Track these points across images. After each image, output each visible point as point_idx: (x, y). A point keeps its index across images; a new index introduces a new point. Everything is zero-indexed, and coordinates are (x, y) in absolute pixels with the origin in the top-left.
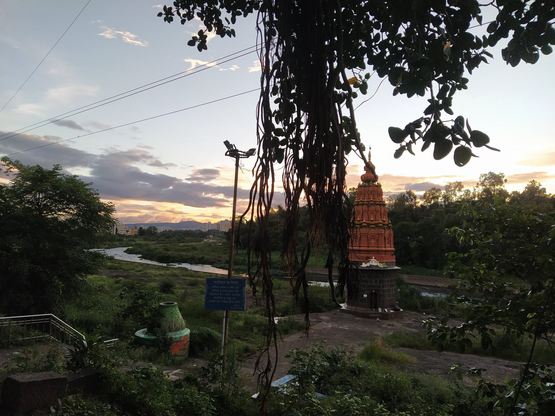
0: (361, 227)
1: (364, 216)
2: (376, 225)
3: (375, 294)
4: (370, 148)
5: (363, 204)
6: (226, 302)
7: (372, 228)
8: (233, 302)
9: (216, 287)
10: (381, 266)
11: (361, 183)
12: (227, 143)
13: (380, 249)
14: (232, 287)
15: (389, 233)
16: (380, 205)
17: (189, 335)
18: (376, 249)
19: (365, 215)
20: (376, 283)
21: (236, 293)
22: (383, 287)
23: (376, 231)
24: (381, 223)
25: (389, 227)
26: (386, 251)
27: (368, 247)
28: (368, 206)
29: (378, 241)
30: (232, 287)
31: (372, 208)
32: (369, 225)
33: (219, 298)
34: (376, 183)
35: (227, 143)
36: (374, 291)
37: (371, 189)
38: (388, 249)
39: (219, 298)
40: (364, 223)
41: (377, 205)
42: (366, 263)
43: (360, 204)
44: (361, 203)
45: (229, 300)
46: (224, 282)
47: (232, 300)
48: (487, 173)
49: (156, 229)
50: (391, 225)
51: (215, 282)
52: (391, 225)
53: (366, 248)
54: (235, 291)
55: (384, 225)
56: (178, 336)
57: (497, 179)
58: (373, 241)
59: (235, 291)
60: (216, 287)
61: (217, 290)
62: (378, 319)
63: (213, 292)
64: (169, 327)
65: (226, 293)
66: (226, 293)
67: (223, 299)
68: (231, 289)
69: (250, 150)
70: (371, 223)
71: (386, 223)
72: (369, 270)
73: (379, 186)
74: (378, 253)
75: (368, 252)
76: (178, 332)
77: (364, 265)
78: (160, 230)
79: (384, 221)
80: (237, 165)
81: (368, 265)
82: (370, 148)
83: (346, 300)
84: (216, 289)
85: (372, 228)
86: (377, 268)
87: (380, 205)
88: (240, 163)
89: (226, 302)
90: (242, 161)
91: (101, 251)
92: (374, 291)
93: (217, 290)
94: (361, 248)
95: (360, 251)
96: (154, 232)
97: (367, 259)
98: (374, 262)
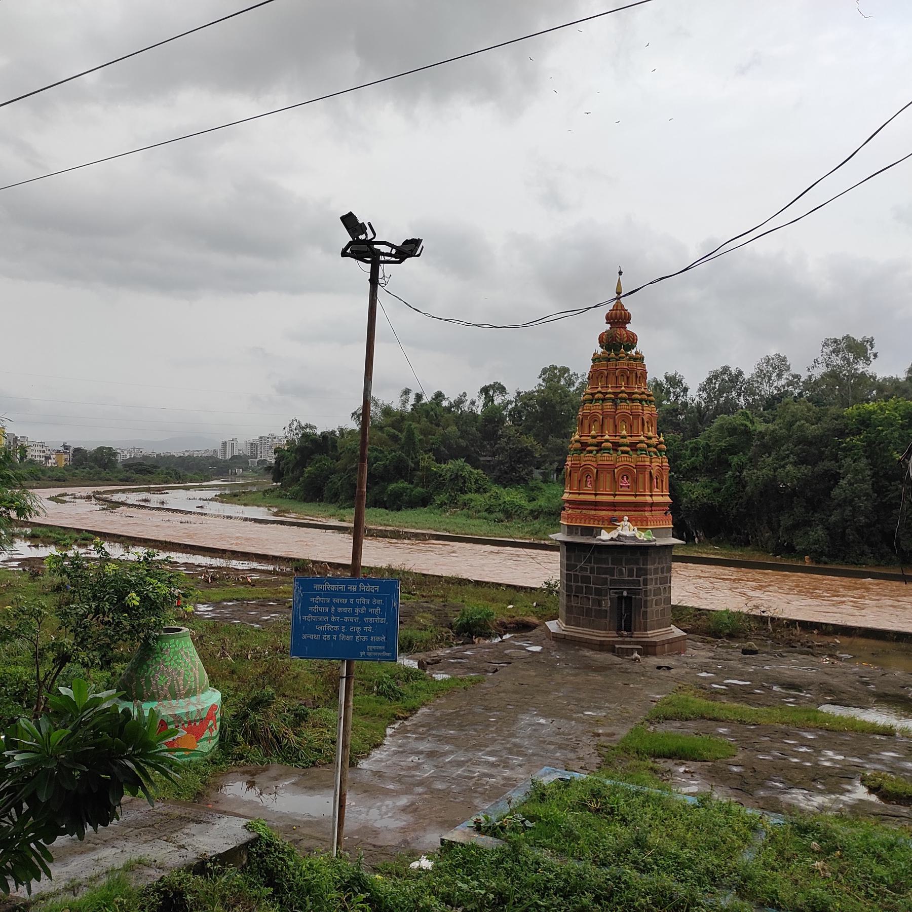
0: (598, 452)
1: (606, 427)
2: (633, 446)
3: (629, 599)
4: (620, 273)
5: (604, 400)
6: (349, 638)
7: (623, 452)
8: (365, 638)
9: (323, 600)
10: (643, 537)
11: (600, 351)
12: (349, 221)
13: (639, 499)
14: (363, 600)
15: (658, 463)
16: (641, 401)
17: (219, 705)
18: (632, 499)
19: (609, 423)
20: (631, 575)
21: (374, 616)
22: (645, 584)
23: (631, 460)
24: (641, 442)
25: (660, 451)
26: (652, 504)
27: (615, 495)
28: (616, 405)
29: (635, 481)
30: (363, 600)
31: (624, 407)
32: (616, 445)
33: (329, 627)
34: (633, 352)
35: (349, 221)
36: (625, 594)
37: (623, 364)
38: (656, 499)
39: (329, 627)
40: (607, 441)
41: (633, 400)
42: (609, 530)
43: (598, 400)
44: (601, 396)
45: (355, 634)
46: (343, 587)
47: (363, 633)
48: (839, 337)
49: (115, 454)
50: (663, 446)
51: (316, 586)
52: (663, 446)
53: (610, 499)
54: (371, 610)
55: (649, 446)
56: (192, 708)
57: (859, 349)
58: (625, 482)
59: (371, 610)
60: (323, 600)
61: (322, 609)
62: (636, 655)
63: (314, 614)
64: (171, 688)
65: (348, 615)
66: (348, 615)
67: (340, 631)
68: (361, 606)
69: (407, 242)
70: (622, 441)
71: (654, 441)
72: (616, 546)
73: (639, 358)
74: (637, 510)
75: (613, 506)
76: (193, 699)
77: (605, 536)
78: (124, 456)
79: (649, 438)
80: (374, 281)
81: (614, 534)
82: (620, 273)
83: (562, 612)
84: (320, 605)
85: (623, 452)
86: (633, 543)
87: (641, 401)
88: (381, 275)
89: (349, 638)
90: (385, 270)
91: (879, 802)
92: (625, 594)
93: (322, 609)
94: (618, 499)
95: (596, 505)
96: (110, 461)
97: (612, 523)
98: (627, 530)
